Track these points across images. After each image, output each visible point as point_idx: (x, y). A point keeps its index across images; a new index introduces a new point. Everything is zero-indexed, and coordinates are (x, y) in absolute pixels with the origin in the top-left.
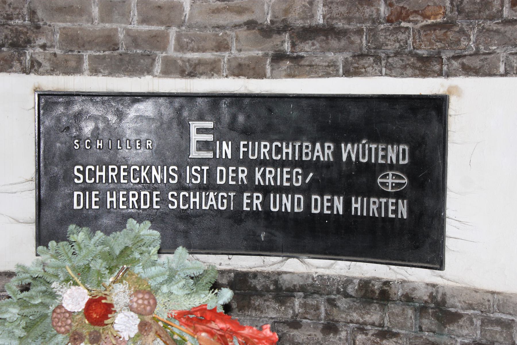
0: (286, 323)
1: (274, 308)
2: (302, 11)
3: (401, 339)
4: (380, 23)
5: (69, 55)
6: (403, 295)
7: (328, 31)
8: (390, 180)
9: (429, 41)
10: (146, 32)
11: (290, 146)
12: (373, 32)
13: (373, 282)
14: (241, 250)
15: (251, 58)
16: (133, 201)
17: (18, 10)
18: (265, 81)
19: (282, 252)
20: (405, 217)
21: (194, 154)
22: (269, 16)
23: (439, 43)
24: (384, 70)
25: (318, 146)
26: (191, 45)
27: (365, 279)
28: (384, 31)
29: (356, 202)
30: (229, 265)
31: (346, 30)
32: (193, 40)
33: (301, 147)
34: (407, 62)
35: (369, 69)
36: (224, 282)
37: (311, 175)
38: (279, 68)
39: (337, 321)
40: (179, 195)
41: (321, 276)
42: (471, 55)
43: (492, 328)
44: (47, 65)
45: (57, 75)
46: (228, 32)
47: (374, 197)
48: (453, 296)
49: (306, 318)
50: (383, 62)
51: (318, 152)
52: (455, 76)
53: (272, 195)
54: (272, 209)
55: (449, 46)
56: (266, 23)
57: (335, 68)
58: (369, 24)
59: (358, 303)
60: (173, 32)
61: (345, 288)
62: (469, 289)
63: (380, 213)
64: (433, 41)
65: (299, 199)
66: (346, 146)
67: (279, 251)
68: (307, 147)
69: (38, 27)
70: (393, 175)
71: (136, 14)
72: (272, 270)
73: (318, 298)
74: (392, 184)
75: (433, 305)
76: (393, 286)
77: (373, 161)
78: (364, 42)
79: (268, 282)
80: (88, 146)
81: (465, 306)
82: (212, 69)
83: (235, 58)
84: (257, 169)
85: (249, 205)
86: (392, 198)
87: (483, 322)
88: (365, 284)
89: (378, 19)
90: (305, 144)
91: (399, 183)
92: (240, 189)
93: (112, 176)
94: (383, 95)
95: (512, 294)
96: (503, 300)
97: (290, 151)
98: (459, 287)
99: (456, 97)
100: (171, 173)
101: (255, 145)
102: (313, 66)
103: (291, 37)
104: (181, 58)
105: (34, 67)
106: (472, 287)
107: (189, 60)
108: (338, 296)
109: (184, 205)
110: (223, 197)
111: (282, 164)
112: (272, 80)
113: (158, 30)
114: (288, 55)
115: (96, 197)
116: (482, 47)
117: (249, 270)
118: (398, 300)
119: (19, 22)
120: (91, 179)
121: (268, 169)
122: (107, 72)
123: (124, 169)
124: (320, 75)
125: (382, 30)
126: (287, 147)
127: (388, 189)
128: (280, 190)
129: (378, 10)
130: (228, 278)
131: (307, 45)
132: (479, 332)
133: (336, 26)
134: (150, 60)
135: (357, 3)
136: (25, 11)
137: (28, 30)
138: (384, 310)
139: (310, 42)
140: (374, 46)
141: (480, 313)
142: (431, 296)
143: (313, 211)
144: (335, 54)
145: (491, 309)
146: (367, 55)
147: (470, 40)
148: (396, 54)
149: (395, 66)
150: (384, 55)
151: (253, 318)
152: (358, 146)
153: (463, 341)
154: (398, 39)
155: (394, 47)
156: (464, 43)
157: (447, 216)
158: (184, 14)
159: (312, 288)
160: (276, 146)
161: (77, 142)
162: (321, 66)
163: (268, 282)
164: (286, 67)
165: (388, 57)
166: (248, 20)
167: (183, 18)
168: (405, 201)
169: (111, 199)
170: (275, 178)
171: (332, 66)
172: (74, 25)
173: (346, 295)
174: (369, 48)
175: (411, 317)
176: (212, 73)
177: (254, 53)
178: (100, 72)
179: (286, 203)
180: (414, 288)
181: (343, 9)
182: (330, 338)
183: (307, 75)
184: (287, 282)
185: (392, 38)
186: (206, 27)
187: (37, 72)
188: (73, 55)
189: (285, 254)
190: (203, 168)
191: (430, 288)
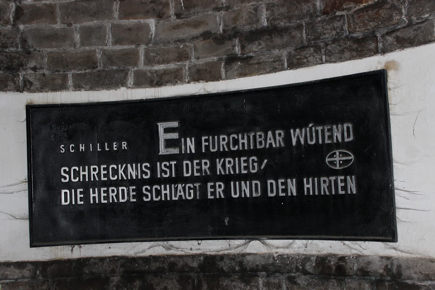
2: (249, 17)
4: (317, 16)
5: (56, 74)
6: (358, 269)
7: (272, 31)
8: (337, 158)
9: (363, 22)
11: (246, 137)
12: (311, 26)
13: (329, 258)
14: (209, 235)
15: (207, 64)
16: (112, 196)
17: (11, 40)
18: (221, 82)
19: (245, 235)
20: (354, 192)
21: (163, 151)
22: (221, 26)
23: (373, 23)
24: (324, 57)
25: (270, 134)
26: (157, 59)
27: (322, 256)
28: (321, 22)
29: (308, 183)
30: (199, 249)
31: (287, 27)
32: (158, 54)
33: (255, 137)
34: (344, 46)
36: (194, 266)
37: (266, 161)
38: (232, 69)
41: (281, 255)
42: (404, 28)
44: (37, 84)
45: (46, 92)
46: (187, 44)
47: (323, 176)
48: (408, 268)
50: (323, 51)
51: (270, 139)
52: (391, 51)
53: (232, 183)
54: (233, 196)
55: (381, 23)
56: (219, 32)
57: (280, 62)
59: (316, 279)
60: (142, 49)
61: (303, 265)
62: (424, 259)
63: (330, 191)
65: (256, 184)
66: (295, 131)
67: (242, 235)
69: (29, 53)
70: (340, 153)
71: (111, 37)
73: (279, 277)
75: (389, 278)
76: (348, 261)
77: (320, 142)
78: (304, 35)
79: (233, 264)
80: (72, 150)
82: (175, 77)
83: (195, 65)
84: (218, 160)
85: (213, 193)
86: (341, 175)
88: (322, 260)
89: (315, 12)
90: (259, 133)
91: (346, 160)
92: (204, 180)
93: (94, 175)
94: (325, 79)
97: (245, 141)
100: (144, 169)
102: (261, 63)
103: (240, 41)
104: (150, 70)
106: (427, 257)
107: (156, 71)
109: (157, 197)
110: (190, 188)
111: (239, 154)
112: (227, 81)
113: (129, 49)
114: (239, 57)
115: (80, 194)
116: (414, 18)
117: (217, 253)
118: (354, 274)
120: (76, 179)
121: (227, 160)
122: (88, 87)
123: (104, 168)
124: (268, 70)
125: (319, 21)
126: (243, 138)
127: (336, 167)
128: (240, 178)
129: (314, 5)
130: (199, 262)
131: (255, 45)
133: (279, 26)
134: (124, 74)
135: (295, 2)
136: (18, 40)
137: (20, 56)
138: (341, 285)
139: (257, 42)
140: (313, 37)
142: (386, 268)
143: (270, 195)
144: (279, 51)
146: (308, 47)
147: (402, 13)
148: (334, 41)
149: (333, 52)
150: (323, 44)
152: (306, 130)
154: (334, 27)
155: (331, 35)
156: (396, 18)
157: (395, 187)
158: (151, 33)
160: (233, 138)
161: (62, 147)
162: (268, 62)
163: (233, 264)
164: (237, 67)
165: (327, 45)
166: (203, 31)
167: (150, 37)
168: (353, 177)
169: (94, 195)
170: (234, 168)
171: (277, 61)
172: (59, 50)
173: (305, 273)
174: (309, 40)
176: (176, 80)
177: (210, 59)
178: (83, 88)
179: (245, 190)
180: (369, 262)
181: (283, 10)
183: (257, 73)
184: (250, 263)
185: (329, 27)
186: (169, 42)
187: (30, 91)
188: (59, 74)
190: (171, 163)
191: (384, 260)
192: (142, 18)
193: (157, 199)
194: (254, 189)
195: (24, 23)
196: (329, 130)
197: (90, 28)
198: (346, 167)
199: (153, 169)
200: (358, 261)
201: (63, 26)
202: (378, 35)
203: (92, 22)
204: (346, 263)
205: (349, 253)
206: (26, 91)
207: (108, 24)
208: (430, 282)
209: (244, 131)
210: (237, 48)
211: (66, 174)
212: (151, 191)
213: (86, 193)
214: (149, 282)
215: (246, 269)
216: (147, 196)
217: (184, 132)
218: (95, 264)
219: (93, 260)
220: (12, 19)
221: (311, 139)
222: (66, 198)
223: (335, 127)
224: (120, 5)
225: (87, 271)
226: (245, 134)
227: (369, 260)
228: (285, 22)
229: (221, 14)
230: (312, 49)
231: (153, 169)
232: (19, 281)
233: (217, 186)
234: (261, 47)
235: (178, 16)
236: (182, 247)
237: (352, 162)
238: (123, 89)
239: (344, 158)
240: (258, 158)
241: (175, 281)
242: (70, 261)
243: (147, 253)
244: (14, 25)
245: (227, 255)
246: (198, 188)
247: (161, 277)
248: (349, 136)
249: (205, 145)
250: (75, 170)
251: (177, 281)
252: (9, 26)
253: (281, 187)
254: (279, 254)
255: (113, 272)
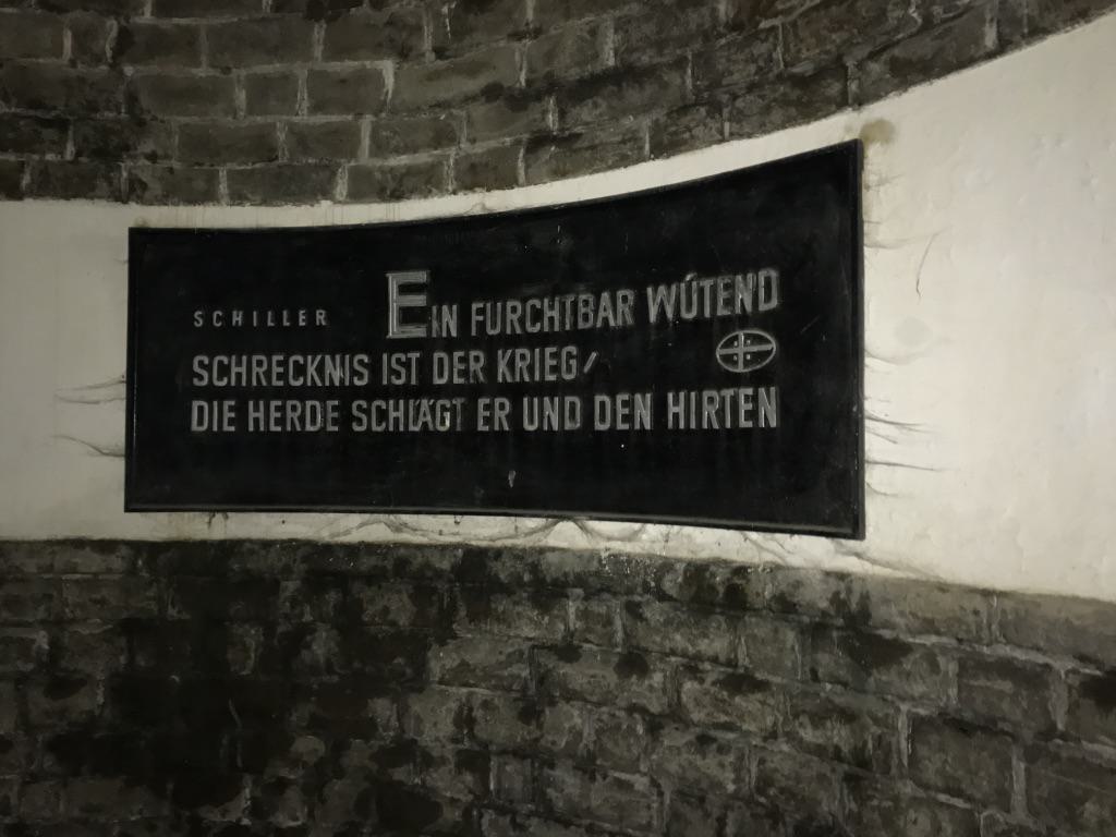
0: (552, 648)
1: (531, 619)
3: (773, 695)
4: (721, 36)
7: (626, 74)
10: (322, 125)
11: (557, 305)
12: (704, 60)
13: (713, 568)
15: (491, 152)
21: (394, 329)
22: (524, 72)
23: (839, 34)
24: (727, 126)
33: (575, 304)
35: (699, 131)
37: (594, 355)
39: (646, 651)
40: (370, 405)
41: (615, 556)
42: (911, 36)
43: (989, 684)
44: (156, 188)
46: (454, 111)
48: (886, 601)
49: (589, 642)
50: (726, 112)
52: (877, 97)
53: (526, 400)
55: (859, 32)
58: (697, 46)
59: (683, 612)
61: (658, 580)
63: (722, 420)
64: (824, 32)
66: (655, 291)
68: (586, 303)
69: (141, 123)
70: (747, 337)
72: (531, 544)
73: (609, 601)
74: (745, 358)
76: (753, 577)
78: (689, 81)
79: (520, 566)
81: (917, 624)
82: (425, 182)
83: (468, 156)
86: (747, 385)
87: (963, 667)
88: (698, 572)
89: (714, 27)
90: (583, 297)
92: (472, 392)
95: (1040, 596)
96: (1016, 611)
98: (902, 579)
99: (878, 145)
101: (496, 307)
103: (558, 102)
104: (380, 167)
105: (134, 192)
106: (932, 579)
107: (392, 169)
108: (648, 596)
109: (379, 423)
110: (444, 409)
111: (541, 340)
112: (529, 188)
114: (555, 137)
116: (937, 10)
117: (491, 543)
119: (110, 115)
120: (222, 380)
121: (519, 352)
124: (610, 162)
125: (722, 46)
128: (542, 390)
129: (714, 10)
131: (585, 109)
132: (953, 692)
133: (638, 64)
136: (120, 97)
139: (590, 102)
140: (706, 83)
141: (954, 642)
142: (835, 599)
143: (599, 426)
145: (985, 634)
146: (696, 104)
148: (751, 88)
150: (727, 96)
151: (497, 638)
152: (678, 288)
153: (914, 710)
154: (753, 55)
155: (744, 74)
157: (866, 414)
158: (385, 90)
159: (603, 579)
163: (520, 566)
165: (735, 97)
170: (531, 369)
171: (630, 140)
173: (662, 596)
175: (793, 648)
178: (247, 199)
179: (550, 415)
180: (798, 582)
181: (649, 29)
182: (632, 684)
185: (741, 57)
187: (141, 200)
189: (550, 512)
191: (832, 580)
192: (367, 59)
193: (379, 429)
194: (567, 414)
195: (134, 62)
196: (727, 287)
197: (265, 77)
198: (758, 367)
199: (375, 368)
200: (774, 579)
201: (212, 72)
202: (850, 63)
203: (271, 66)
204: (748, 581)
205: (756, 560)
206: (133, 200)
207: (301, 71)
208: (934, 639)
209: (556, 291)
210: (550, 116)
211: (204, 370)
212: (367, 412)
213: (241, 411)
214: (357, 596)
215: (544, 579)
216: (360, 421)
217: (438, 292)
218: (252, 552)
219: (248, 545)
220: (109, 54)
221: (689, 308)
222: (203, 418)
223: (739, 278)
224: (326, 30)
225: (236, 567)
226: (557, 299)
227: (798, 578)
228: (652, 54)
229: (525, 45)
230: (703, 110)
231: (375, 368)
232: (100, 577)
233: (497, 405)
234: (598, 112)
235: (440, 52)
236: (424, 528)
237: (771, 357)
238: (326, 204)
239: (755, 349)
240: (579, 351)
241: (405, 597)
242: (203, 544)
243: (355, 537)
244: (113, 66)
245: (510, 548)
246: (459, 407)
247: (380, 587)
248: (768, 298)
249: (477, 322)
250: (220, 363)
251: (410, 597)
252: (104, 68)
253: (621, 411)
254: (612, 552)
255: (287, 571)
